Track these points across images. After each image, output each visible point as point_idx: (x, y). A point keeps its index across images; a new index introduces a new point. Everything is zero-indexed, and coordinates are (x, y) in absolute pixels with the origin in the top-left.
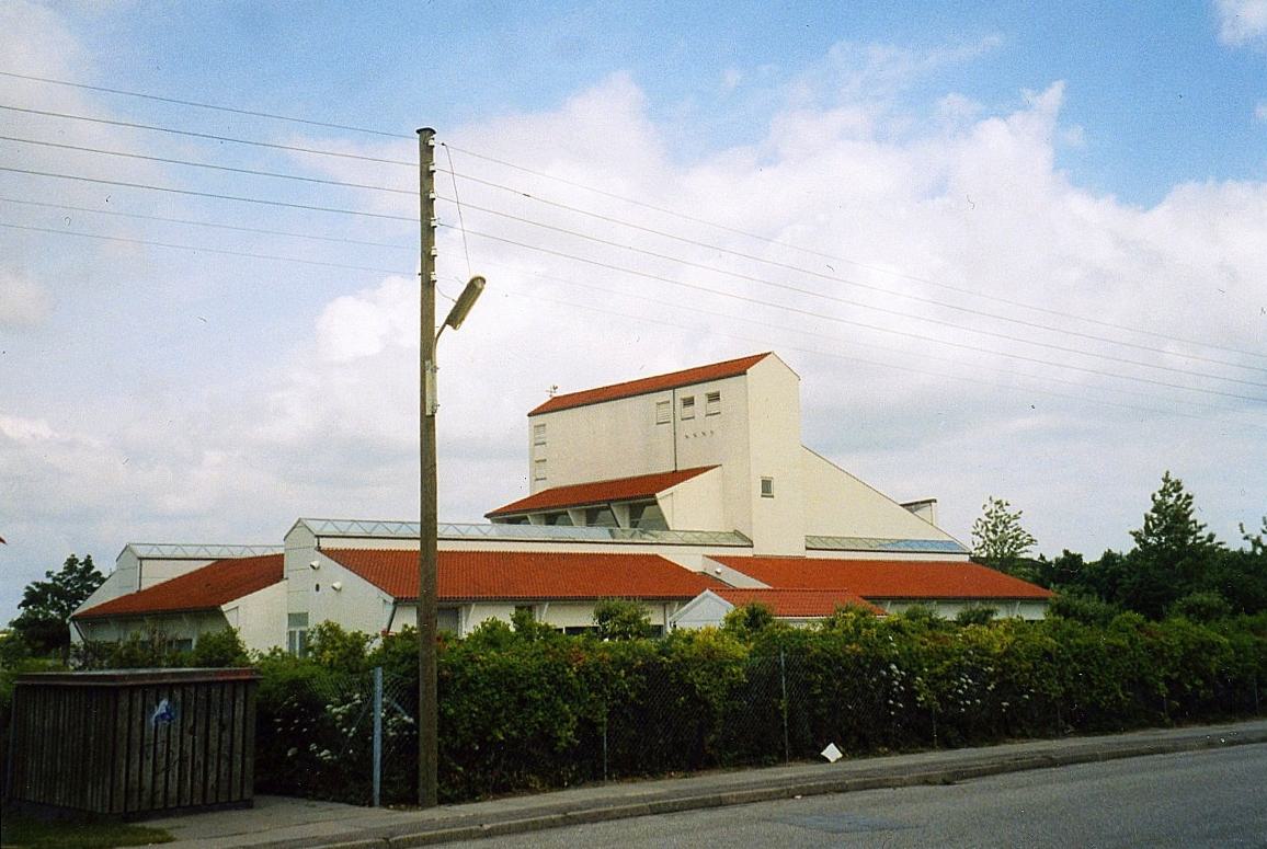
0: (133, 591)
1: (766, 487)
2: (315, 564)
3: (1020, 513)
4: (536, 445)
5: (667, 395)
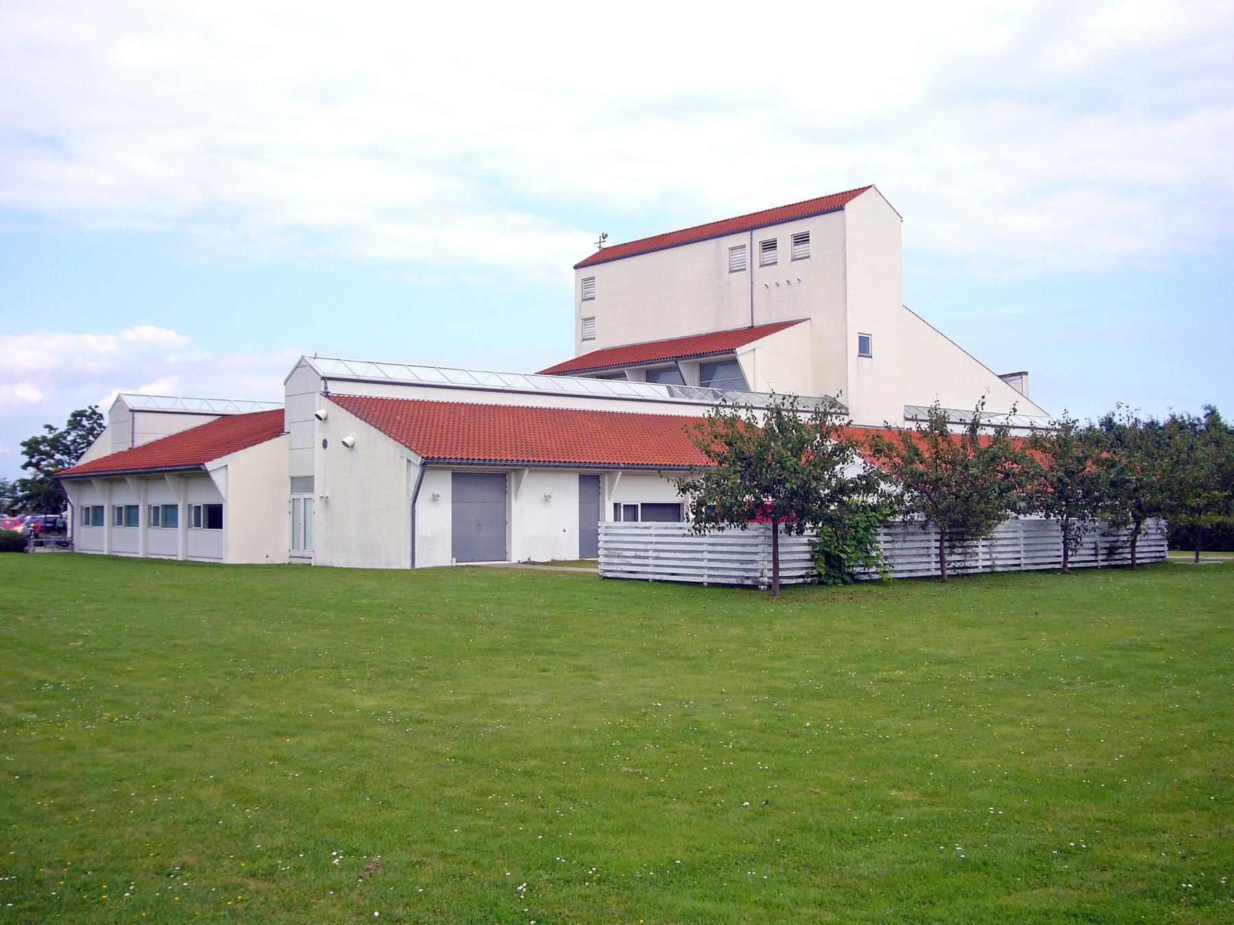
0: (124, 448)
1: (864, 345)
2: (322, 413)
3: (983, 397)
4: (583, 300)
5: (742, 239)
